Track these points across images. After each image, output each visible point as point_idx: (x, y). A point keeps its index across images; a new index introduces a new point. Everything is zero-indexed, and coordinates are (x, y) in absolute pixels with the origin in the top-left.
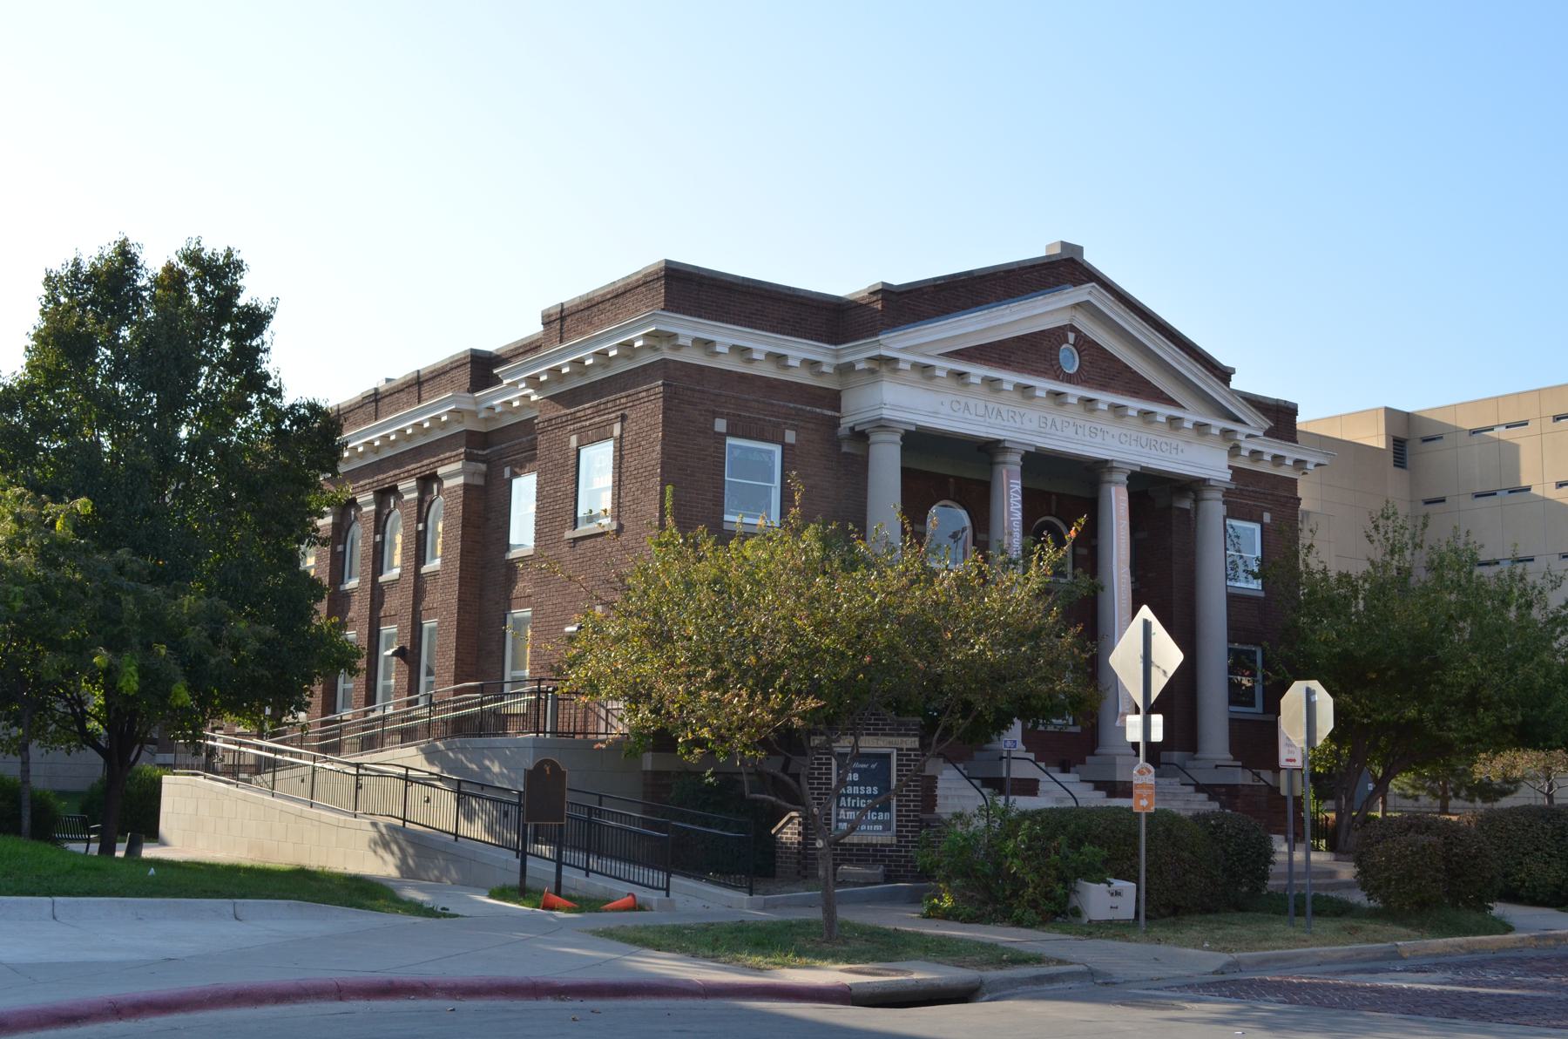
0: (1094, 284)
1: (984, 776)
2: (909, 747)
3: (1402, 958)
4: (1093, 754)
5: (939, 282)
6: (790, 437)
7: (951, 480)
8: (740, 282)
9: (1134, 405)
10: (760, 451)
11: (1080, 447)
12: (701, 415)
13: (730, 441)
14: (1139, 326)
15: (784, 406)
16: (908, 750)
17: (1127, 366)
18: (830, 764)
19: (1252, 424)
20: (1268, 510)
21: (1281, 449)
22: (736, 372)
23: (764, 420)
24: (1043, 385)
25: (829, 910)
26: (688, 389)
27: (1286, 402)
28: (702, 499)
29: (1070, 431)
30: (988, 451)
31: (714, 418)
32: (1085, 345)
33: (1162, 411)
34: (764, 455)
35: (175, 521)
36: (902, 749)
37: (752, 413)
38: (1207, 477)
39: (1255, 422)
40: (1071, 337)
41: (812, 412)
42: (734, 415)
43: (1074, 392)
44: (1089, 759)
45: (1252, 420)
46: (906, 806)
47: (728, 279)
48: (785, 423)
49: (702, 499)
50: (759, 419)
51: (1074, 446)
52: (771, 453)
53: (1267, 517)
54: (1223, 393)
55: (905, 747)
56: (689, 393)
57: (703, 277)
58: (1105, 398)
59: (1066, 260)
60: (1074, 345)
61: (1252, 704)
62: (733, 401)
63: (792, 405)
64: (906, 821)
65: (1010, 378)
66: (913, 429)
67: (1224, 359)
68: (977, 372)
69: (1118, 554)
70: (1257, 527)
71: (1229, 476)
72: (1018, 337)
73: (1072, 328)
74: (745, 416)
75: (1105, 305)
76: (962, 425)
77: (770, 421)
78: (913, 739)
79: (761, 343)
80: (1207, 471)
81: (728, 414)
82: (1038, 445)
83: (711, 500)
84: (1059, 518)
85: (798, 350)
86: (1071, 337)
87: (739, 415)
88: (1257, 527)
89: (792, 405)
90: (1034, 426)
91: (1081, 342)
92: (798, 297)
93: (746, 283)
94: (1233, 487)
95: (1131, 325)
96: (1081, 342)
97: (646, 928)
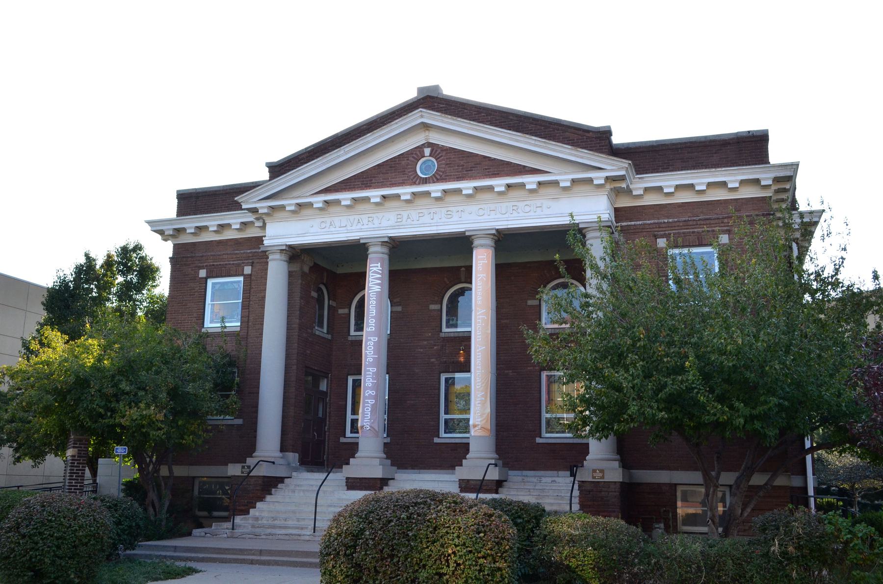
0: (420, 109)
4: (354, 457)
6: (203, 273)
7: (463, 269)
8: (222, 189)
9: (499, 183)
10: (232, 282)
11: (435, 228)
12: (192, 270)
13: (671, 252)
14: (478, 128)
15: (244, 253)
17: (485, 157)
18: (84, 470)
22: (215, 241)
23: (230, 264)
24: (405, 191)
26: (183, 257)
27: (749, 132)
28: (191, 317)
29: (426, 219)
32: (437, 151)
33: (531, 181)
34: (235, 285)
37: (225, 261)
38: (463, 230)
39: (613, 166)
40: (427, 151)
42: (210, 265)
43: (436, 189)
44: (351, 460)
48: (243, 263)
49: (191, 317)
50: (226, 264)
51: (429, 229)
52: (213, 284)
56: (184, 259)
57: (199, 193)
58: (467, 186)
59: (423, 99)
62: (211, 257)
63: (249, 251)
65: (375, 194)
67: (592, 120)
68: (345, 197)
69: (476, 301)
70: (210, 282)
72: (378, 165)
74: (217, 265)
76: (547, 220)
77: (233, 264)
79: (701, 179)
81: (206, 266)
82: (497, 228)
83: (196, 317)
85: (235, 218)
86: (427, 151)
88: (210, 282)
89: (249, 251)
90: (391, 223)
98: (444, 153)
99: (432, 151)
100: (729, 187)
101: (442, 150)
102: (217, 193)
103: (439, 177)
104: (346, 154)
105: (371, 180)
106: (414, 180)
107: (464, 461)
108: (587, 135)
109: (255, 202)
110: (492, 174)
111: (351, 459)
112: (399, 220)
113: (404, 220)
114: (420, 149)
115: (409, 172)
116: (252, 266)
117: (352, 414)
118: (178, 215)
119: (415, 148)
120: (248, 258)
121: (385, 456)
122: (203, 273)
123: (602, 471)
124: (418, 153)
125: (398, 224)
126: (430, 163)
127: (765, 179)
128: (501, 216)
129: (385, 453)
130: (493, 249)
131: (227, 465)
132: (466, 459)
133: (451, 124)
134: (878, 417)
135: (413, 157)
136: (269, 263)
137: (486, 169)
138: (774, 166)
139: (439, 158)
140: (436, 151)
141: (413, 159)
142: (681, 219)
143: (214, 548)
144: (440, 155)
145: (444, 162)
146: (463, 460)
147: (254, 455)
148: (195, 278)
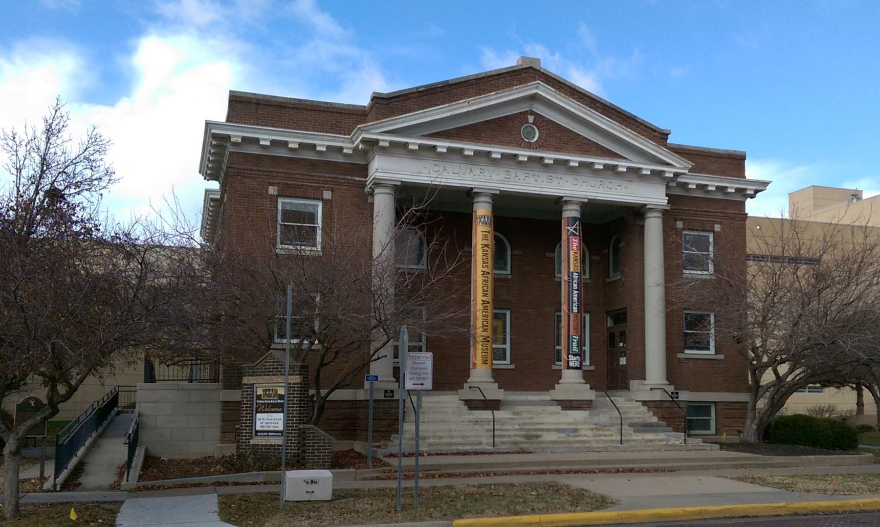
1: (465, 399)
2: (294, 382)
3: (839, 514)
5: (421, 89)
16: (293, 384)
19: (678, 165)
20: (718, 223)
21: (306, 136)
25: (417, 483)
30: (469, 195)
31: (676, 221)
33: (599, 162)
35: (821, 308)
36: (290, 384)
39: (680, 164)
40: (531, 119)
41: (353, 180)
45: (677, 162)
46: (291, 420)
47: (279, 100)
53: (272, 190)
54: (652, 146)
55: (292, 381)
60: (533, 123)
61: (708, 349)
64: (292, 430)
65: (470, 148)
66: (498, 192)
71: (666, 201)
72: (486, 121)
73: (532, 113)
74: (291, 185)
75: (550, 95)
77: (311, 186)
78: (297, 377)
80: (644, 199)
81: (278, 183)
84: (503, 234)
86: (531, 119)
87: (287, 184)
91: (540, 121)
92: (333, 108)
93: (293, 102)
94: (669, 208)
95: (572, 107)
96: (540, 121)
97: (352, 489)
98: (544, 124)
99: (535, 120)
100: (289, 146)
101: (543, 121)
102: (283, 105)
103: (541, 144)
104: (470, 106)
105: (480, 134)
106: (520, 143)
107: (556, 385)
108: (654, 133)
109: (378, 134)
110: (585, 151)
111: (673, 386)
112: (508, 176)
113: (512, 178)
114: (525, 114)
115: (515, 134)
116: (332, 191)
117: (506, 349)
118: (228, 120)
119: (521, 113)
120: (326, 183)
121: (492, 380)
122: (327, 195)
123: (392, 391)
124: (523, 118)
125: (506, 180)
126: (530, 129)
127: (320, 145)
128: (591, 188)
129: (493, 378)
130: (490, 205)
131: (457, 390)
132: (559, 384)
133: (562, 101)
134: (312, 343)
135: (518, 121)
136: (375, 196)
137: (578, 145)
138: (865, 200)
139: (540, 127)
140: (538, 120)
141: (518, 123)
142: (346, 177)
143: (476, 464)
144: (541, 125)
145: (545, 131)
146: (465, 384)
147: (560, 381)
148: (264, 195)
